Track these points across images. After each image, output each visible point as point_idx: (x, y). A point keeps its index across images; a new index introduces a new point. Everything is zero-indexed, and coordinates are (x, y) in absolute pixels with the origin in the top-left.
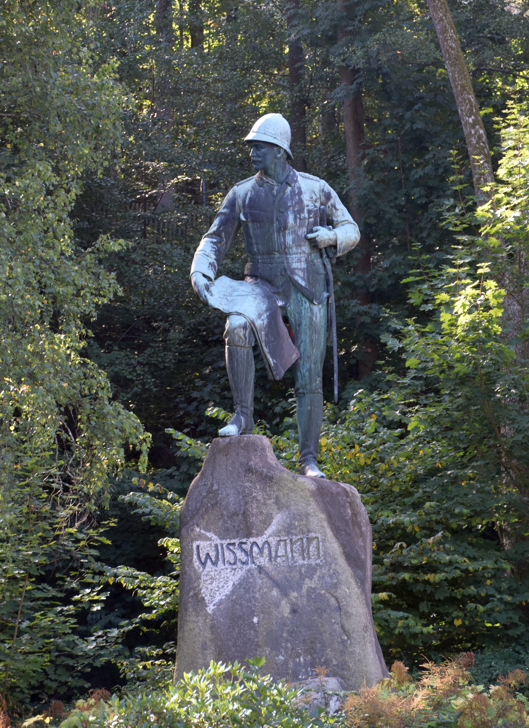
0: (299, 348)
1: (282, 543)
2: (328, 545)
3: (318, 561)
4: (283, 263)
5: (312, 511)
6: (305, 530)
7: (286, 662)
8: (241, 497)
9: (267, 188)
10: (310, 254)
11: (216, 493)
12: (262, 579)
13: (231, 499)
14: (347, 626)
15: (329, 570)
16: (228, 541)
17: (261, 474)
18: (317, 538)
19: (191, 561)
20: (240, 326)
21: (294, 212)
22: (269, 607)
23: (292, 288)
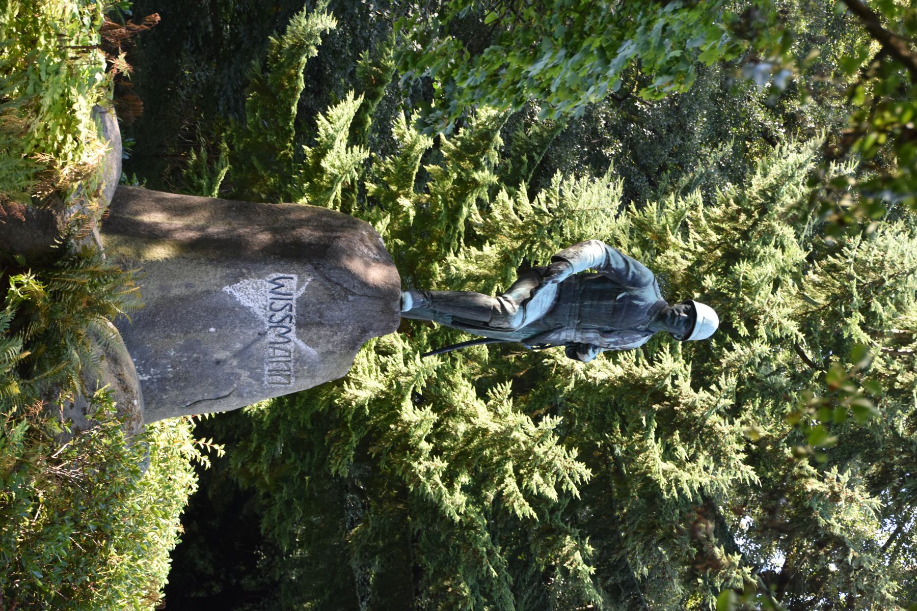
1: (287, 354)
3: (266, 383)
7: (167, 357)
11: (345, 298)
12: (253, 335)
16: (294, 305)
17: (359, 340)
19: (278, 271)
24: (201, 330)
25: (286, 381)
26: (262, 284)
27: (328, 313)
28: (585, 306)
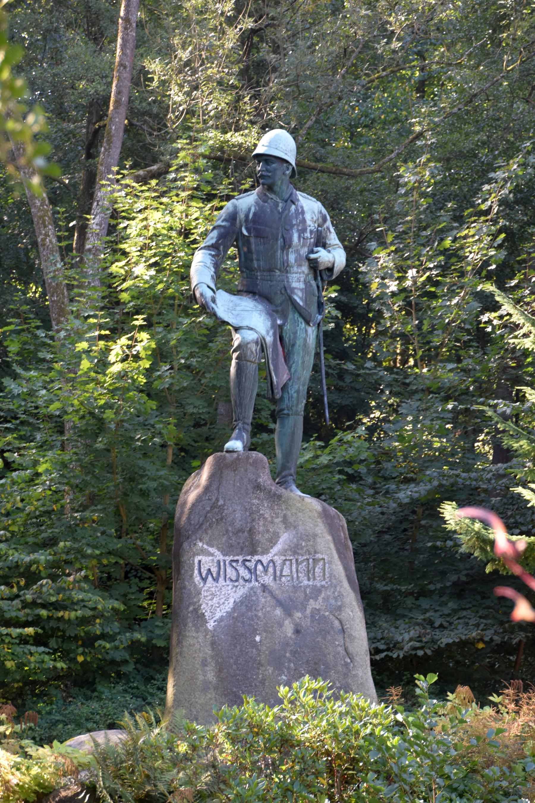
0: (290, 368)
1: (288, 563)
2: (334, 567)
3: (323, 583)
4: (283, 281)
5: (319, 532)
6: (312, 550)
8: (248, 514)
9: (272, 204)
10: (307, 275)
12: (265, 598)
13: (238, 515)
14: (350, 649)
15: (334, 593)
16: (231, 558)
17: (270, 492)
18: (324, 559)
19: (192, 576)
20: (253, 341)
21: (298, 230)
22: (272, 627)
23: (290, 307)
24: (258, 650)
25: (321, 563)
26: (207, 591)
27: (238, 524)
28: (259, 266)
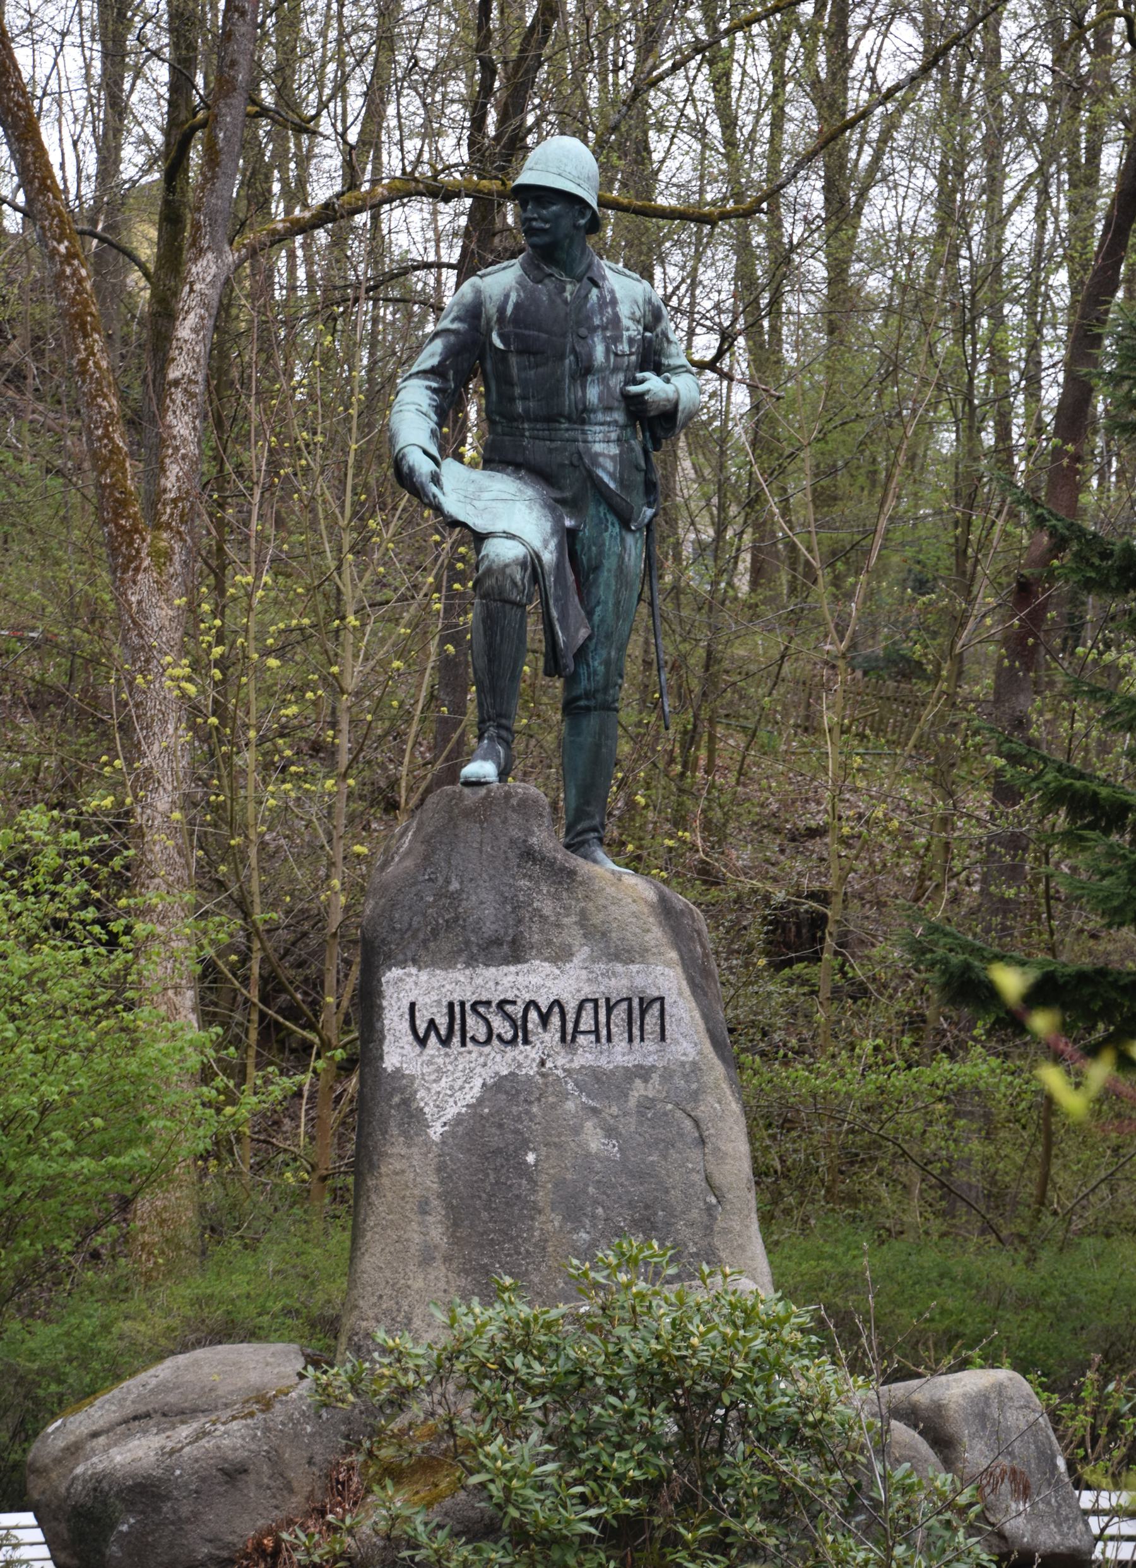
1: (589, 1006)
8: (509, 908)
11: (455, 897)
14: (718, 1179)
17: (552, 864)
21: (605, 338)
27: (489, 928)
